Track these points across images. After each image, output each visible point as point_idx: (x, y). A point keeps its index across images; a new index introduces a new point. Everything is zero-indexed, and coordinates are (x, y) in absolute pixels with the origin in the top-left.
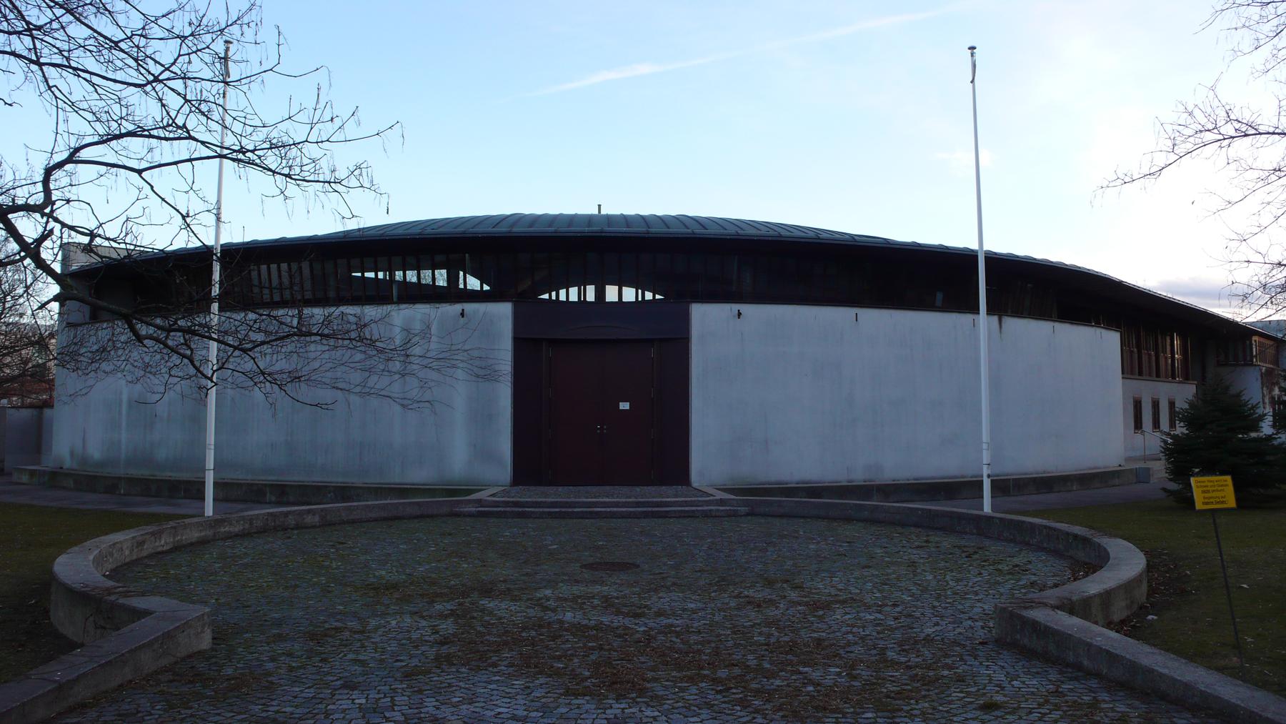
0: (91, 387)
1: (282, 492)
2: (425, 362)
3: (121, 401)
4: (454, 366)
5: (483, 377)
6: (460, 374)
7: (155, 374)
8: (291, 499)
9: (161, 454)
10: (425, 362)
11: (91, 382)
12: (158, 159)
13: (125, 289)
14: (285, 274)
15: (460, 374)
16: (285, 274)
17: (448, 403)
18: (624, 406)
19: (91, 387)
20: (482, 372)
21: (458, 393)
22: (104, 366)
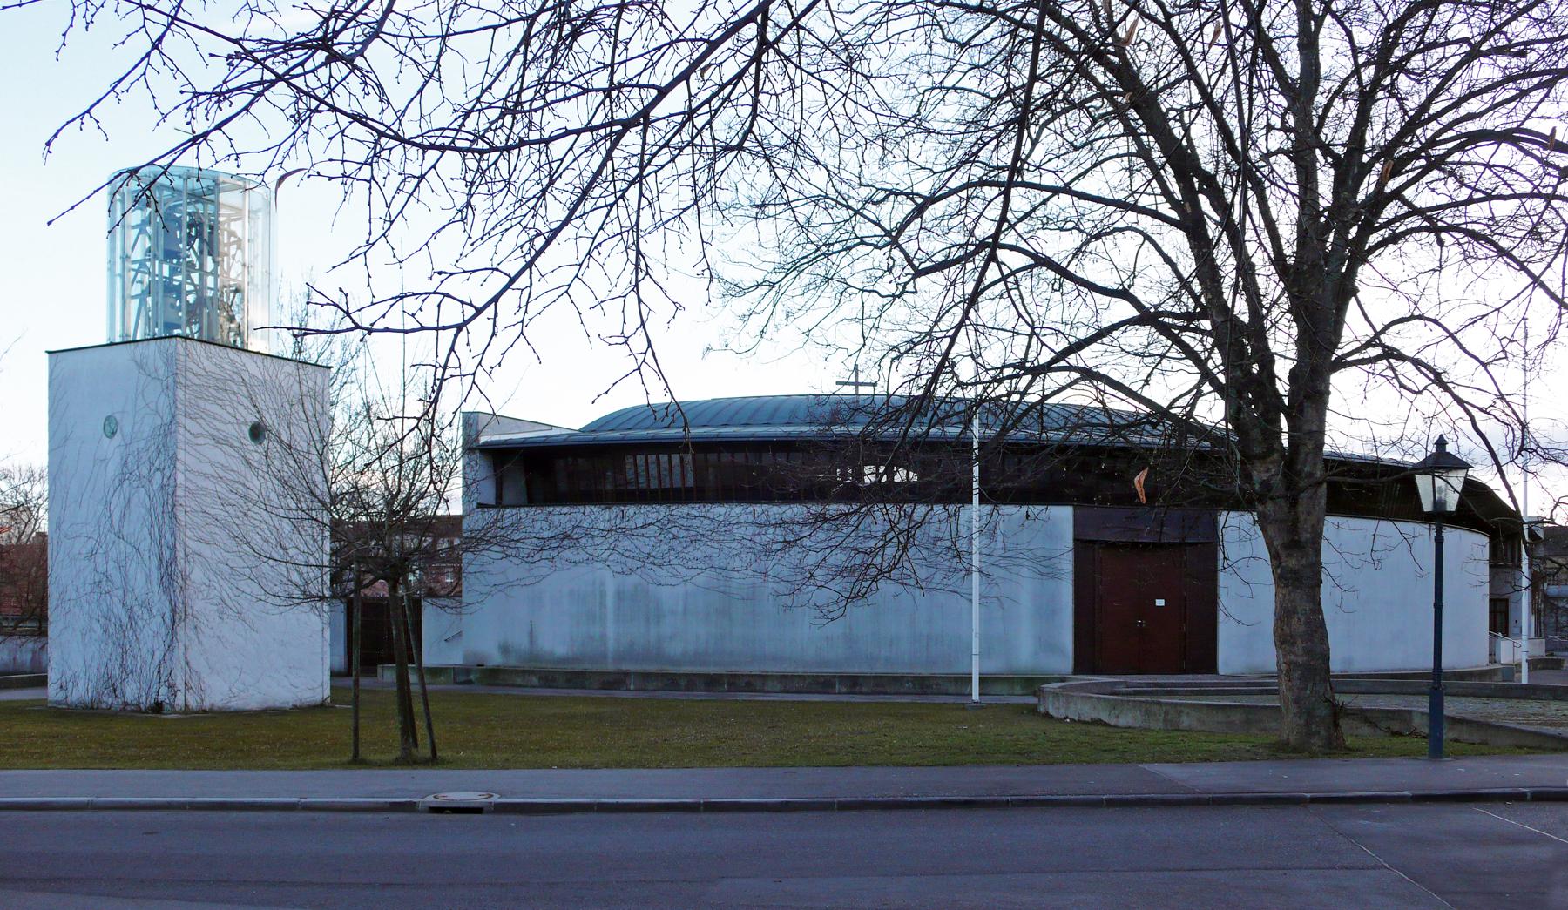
0: (543, 577)
1: (854, 682)
2: (992, 560)
3: (603, 595)
4: (1019, 565)
5: (1047, 575)
6: (1025, 572)
7: (660, 566)
8: (864, 689)
9: (675, 648)
10: (992, 560)
11: (544, 571)
12: (1533, 106)
13: (540, 472)
14: (653, 470)
15: (1025, 572)
16: (653, 470)
17: (1001, 595)
18: (1160, 603)
19: (543, 577)
20: (1046, 570)
21: (1024, 588)
22: (568, 554)
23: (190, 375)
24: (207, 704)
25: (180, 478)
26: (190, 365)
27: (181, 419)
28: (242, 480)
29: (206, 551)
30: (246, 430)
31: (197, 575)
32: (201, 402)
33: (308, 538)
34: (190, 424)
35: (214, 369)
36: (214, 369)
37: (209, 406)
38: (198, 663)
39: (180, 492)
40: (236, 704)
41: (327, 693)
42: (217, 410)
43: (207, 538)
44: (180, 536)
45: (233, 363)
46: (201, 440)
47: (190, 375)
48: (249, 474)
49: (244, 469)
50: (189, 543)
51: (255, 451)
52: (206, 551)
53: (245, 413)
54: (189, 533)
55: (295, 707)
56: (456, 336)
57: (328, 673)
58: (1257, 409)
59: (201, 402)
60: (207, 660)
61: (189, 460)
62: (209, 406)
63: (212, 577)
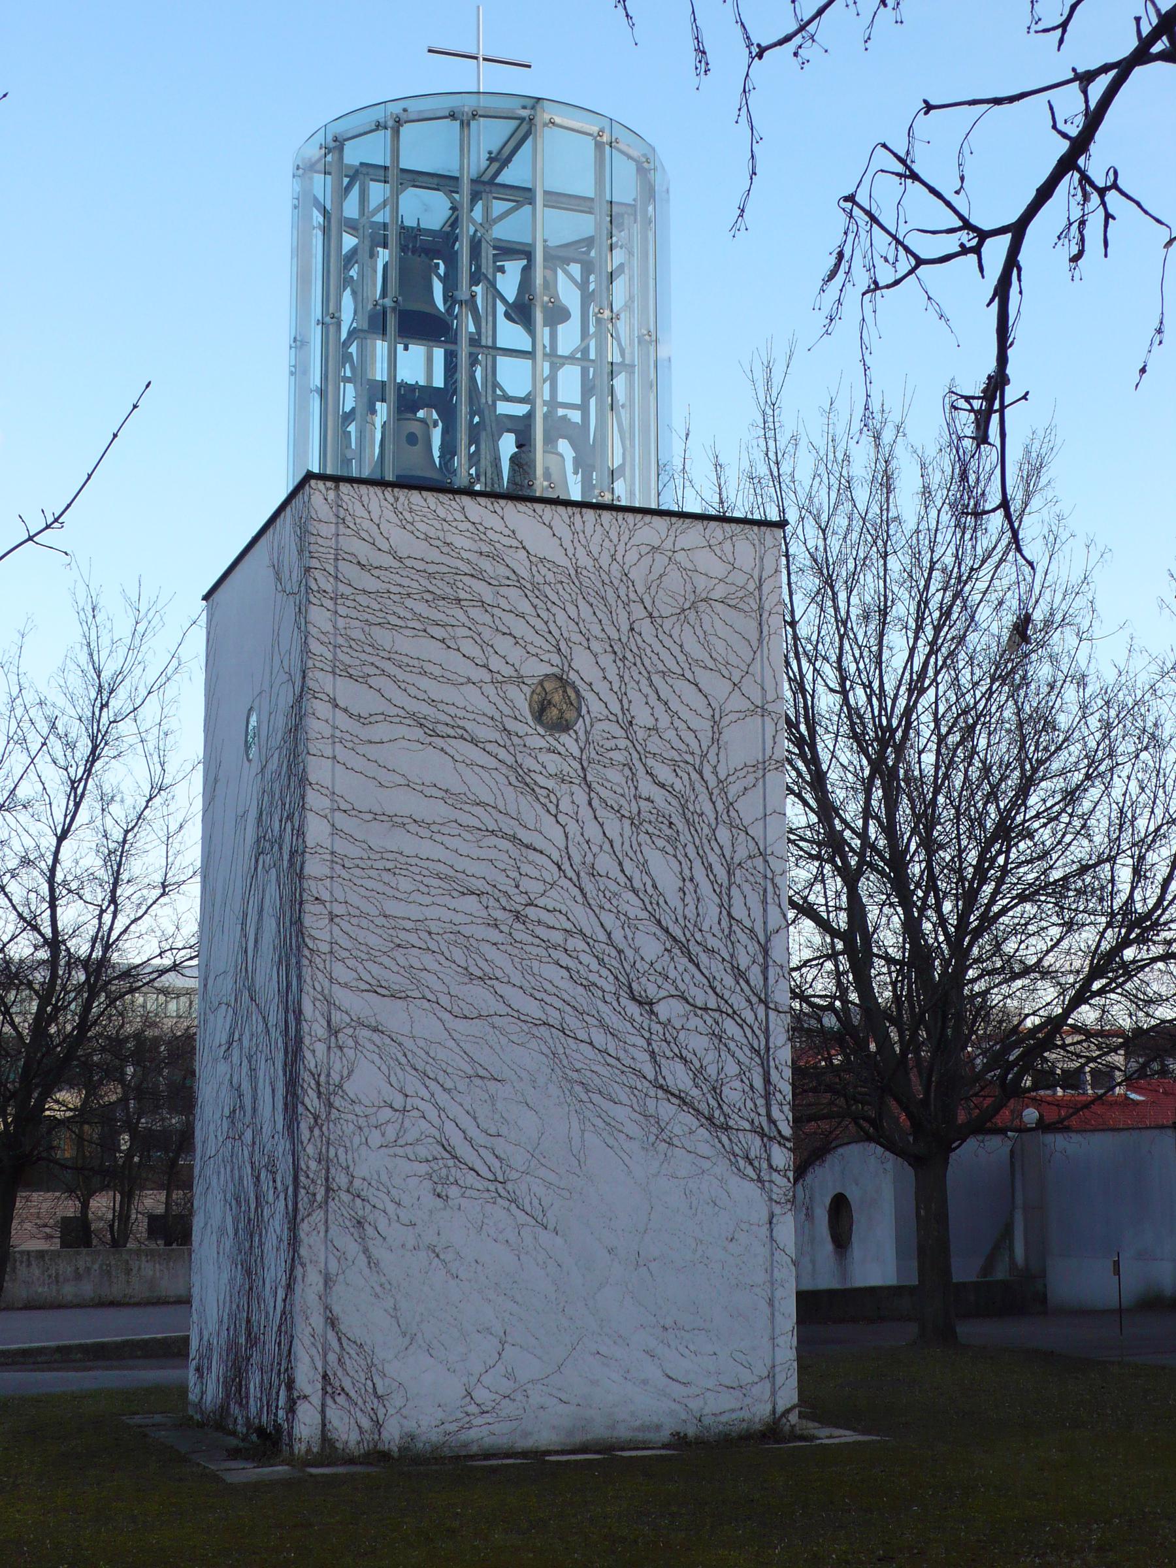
23: (348, 570)
24: (392, 1435)
25: (316, 831)
26: (353, 545)
27: (322, 680)
28: (508, 826)
29: (394, 1016)
30: (521, 699)
31: (366, 1081)
32: (382, 636)
33: (716, 968)
34: (345, 691)
35: (420, 549)
36: (420, 549)
37: (406, 644)
38: (364, 1316)
39: (314, 867)
40: (484, 1433)
41: (788, 1395)
42: (431, 650)
43: (397, 981)
44: (314, 981)
45: (478, 530)
46: (381, 731)
47: (348, 570)
48: (528, 809)
49: (513, 800)
50: (341, 996)
51: (550, 755)
52: (394, 1016)
53: (516, 655)
54: (340, 972)
55: (680, 1441)
56: (773, 1360)
57: (789, 1307)
58: (971, 1058)
59: (382, 636)
60: (395, 1313)
61: (346, 783)
62: (406, 644)
63: (413, 1084)
